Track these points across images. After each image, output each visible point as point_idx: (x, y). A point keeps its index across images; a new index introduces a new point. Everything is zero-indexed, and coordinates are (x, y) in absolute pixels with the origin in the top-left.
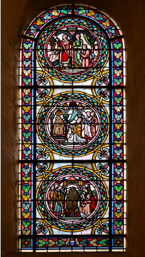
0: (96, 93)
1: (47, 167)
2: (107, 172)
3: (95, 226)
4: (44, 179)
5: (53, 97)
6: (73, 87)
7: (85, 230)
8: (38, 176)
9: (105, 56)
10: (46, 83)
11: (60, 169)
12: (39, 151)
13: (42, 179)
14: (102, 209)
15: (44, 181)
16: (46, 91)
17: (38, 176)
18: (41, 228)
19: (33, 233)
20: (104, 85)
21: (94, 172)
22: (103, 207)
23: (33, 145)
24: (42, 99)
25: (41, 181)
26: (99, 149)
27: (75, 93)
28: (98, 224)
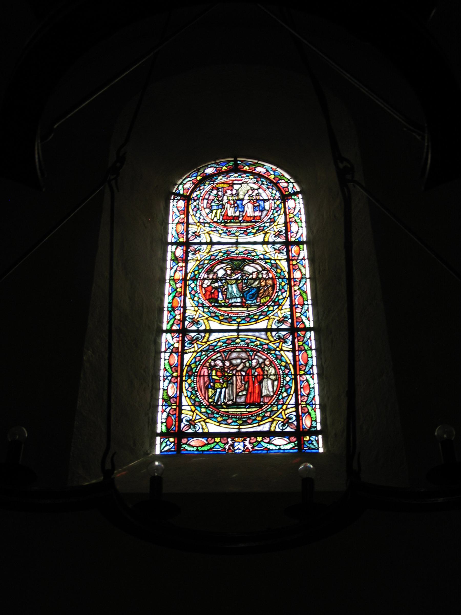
0: (204, 323)
1: (279, 425)
2: (184, 420)
3: (204, 342)
4: (284, 407)
5: (270, 420)
6: (238, 331)
7: (219, 338)
8: (292, 412)
9: (188, 389)
10: (277, 334)
11: (257, 321)
12: (292, 418)
13: (287, 407)
14: (193, 366)
15: (283, 404)
16: (281, 428)
17: (292, 412)
18: (288, 422)
19: (288, 234)
20: (193, 334)
21: (205, 420)
22: (192, 369)
23: (292, 277)
24: (287, 416)
25: (288, 404)
26: (198, 417)
27: (236, 324)
28: (201, 316)
